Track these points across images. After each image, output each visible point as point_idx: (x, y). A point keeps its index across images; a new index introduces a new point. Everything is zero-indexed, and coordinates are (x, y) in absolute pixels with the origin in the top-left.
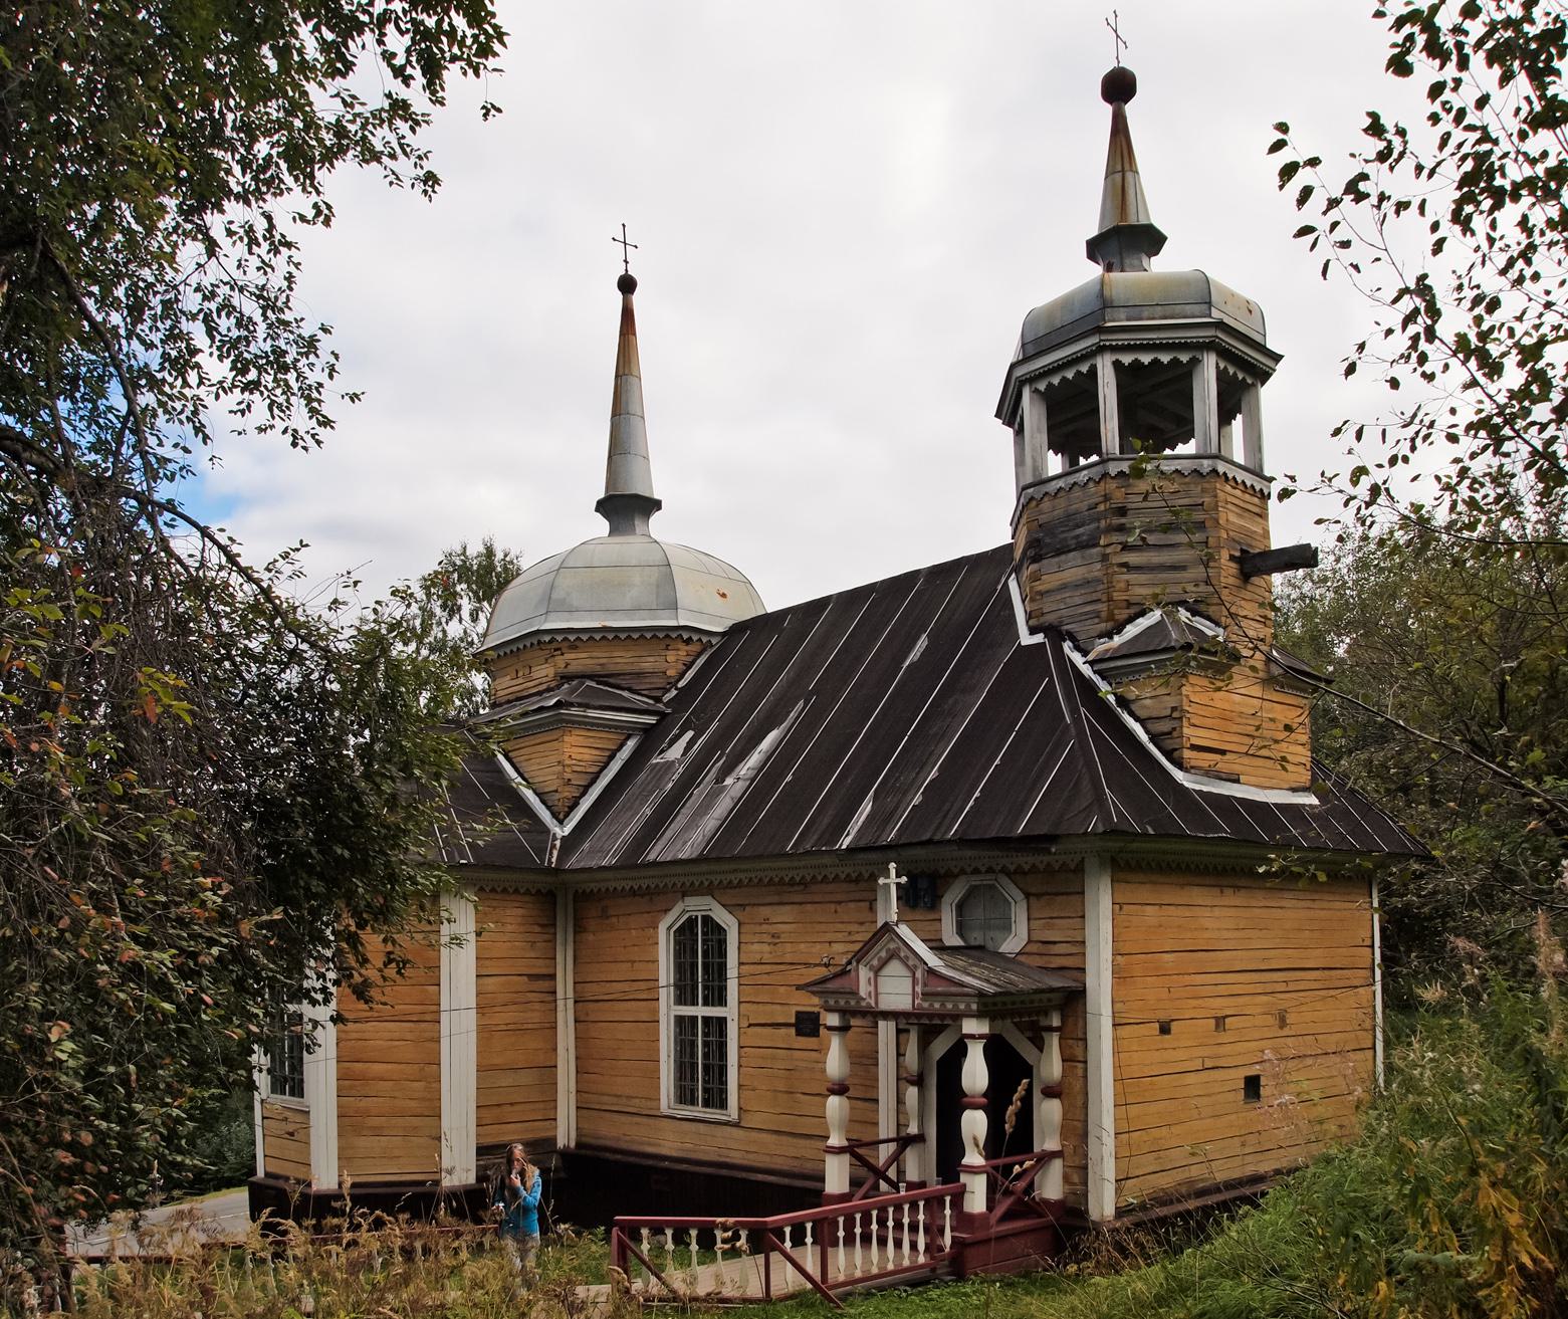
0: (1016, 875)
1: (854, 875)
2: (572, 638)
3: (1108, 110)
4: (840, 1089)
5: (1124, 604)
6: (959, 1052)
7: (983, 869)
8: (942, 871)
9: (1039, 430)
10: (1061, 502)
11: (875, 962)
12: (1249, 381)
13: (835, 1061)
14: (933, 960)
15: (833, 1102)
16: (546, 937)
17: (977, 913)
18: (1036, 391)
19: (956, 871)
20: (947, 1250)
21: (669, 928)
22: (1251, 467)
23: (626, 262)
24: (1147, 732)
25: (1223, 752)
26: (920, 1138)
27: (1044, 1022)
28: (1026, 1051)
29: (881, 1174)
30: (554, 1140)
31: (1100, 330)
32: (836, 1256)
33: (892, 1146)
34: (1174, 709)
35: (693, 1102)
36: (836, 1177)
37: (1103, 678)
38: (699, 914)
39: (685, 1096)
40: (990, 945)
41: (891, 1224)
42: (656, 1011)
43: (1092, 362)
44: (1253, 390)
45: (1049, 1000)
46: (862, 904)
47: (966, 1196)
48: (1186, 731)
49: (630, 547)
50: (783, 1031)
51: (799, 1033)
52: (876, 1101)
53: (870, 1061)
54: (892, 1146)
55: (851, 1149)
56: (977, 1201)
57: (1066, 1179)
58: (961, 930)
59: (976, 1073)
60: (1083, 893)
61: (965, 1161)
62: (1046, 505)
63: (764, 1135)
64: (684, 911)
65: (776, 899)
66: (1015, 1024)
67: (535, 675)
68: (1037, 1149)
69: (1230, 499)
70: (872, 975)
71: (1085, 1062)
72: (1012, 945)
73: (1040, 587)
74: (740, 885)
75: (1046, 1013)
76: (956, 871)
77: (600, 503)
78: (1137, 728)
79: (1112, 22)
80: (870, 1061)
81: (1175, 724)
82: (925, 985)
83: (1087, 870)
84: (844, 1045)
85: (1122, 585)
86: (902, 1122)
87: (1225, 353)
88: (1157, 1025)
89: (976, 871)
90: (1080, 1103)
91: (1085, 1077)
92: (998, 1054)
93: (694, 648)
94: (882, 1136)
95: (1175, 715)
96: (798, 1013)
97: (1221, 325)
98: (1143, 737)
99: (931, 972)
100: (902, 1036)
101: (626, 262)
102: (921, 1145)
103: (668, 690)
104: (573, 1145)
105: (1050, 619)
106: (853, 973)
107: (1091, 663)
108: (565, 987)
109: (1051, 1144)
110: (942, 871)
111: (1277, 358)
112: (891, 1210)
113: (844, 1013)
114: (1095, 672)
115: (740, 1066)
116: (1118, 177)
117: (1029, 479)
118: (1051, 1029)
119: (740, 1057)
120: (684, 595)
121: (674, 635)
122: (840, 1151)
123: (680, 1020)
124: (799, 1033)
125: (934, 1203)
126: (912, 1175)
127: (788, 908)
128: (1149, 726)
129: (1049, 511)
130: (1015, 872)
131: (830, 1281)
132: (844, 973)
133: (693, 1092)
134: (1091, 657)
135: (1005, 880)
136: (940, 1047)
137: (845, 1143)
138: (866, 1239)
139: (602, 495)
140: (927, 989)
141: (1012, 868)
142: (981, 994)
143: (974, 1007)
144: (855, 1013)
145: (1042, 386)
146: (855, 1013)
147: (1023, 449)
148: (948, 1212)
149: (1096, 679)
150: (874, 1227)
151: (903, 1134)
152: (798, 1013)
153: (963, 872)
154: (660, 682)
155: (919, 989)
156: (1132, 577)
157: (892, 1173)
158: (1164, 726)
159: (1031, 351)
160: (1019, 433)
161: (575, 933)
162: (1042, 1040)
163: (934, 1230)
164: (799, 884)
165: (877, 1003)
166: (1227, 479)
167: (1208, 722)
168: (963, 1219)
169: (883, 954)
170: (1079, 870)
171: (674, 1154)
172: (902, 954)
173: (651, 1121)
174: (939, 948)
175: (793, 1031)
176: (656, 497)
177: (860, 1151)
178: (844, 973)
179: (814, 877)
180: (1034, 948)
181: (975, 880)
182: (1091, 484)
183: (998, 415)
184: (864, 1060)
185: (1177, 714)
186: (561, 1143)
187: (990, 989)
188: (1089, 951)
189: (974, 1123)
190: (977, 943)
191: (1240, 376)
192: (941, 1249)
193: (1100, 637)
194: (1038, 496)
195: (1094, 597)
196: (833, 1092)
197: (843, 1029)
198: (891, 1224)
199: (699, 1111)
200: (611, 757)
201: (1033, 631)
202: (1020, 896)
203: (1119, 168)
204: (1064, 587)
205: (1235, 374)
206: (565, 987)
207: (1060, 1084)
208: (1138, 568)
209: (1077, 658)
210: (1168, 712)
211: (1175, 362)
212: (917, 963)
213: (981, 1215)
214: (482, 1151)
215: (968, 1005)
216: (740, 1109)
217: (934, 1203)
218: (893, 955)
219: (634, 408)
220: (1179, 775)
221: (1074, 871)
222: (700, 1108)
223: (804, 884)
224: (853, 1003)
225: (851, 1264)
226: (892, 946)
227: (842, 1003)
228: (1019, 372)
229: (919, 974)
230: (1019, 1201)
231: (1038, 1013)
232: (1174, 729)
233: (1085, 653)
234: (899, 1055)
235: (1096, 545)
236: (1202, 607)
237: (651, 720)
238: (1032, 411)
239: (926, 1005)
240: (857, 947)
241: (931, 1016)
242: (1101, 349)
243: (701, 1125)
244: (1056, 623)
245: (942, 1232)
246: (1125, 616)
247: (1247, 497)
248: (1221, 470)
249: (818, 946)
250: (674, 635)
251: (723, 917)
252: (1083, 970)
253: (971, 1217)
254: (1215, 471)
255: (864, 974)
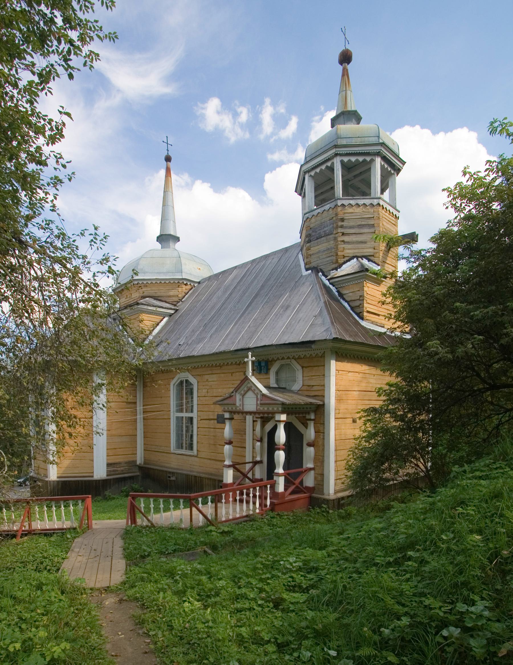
0: (298, 359)
1: (238, 362)
2: (145, 282)
3: (340, 68)
4: (230, 443)
5: (342, 257)
6: (275, 429)
7: (286, 358)
8: (270, 359)
9: (311, 192)
10: (319, 218)
11: (242, 392)
12: (392, 172)
13: (227, 430)
14: (265, 391)
15: (227, 447)
16: (133, 389)
17: (283, 375)
18: (311, 176)
19: (275, 359)
20: (268, 507)
21: (174, 385)
22: (391, 204)
23: (168, 150)
24: (350, 306)
25: (379, 315)
26: (261, 462)
27: (308, 417)
28: (300, 427)
29: (245, 476)
30: (136, 461)
31: (336, 146)
32: (222, 508)
33: (251, 465)
34: (360, 296)
35: (182, 448)
36: (229, 476)
37: (334, 286)
38: (184, 379)
39: (180, 446)
40: (288, 388)
41: (251, 495)
42: (169, 415)
43: (332, 161)
44: (393, 176)
45: (310, 408)
46: (241, 373)
47: (276, 485)
48: (365, 305)
49: (167, 252)
50: (212, 421)
51: (218, 422)
52: (245, 448)
53: (243, 433)
54: (251, 465)
55: (233, 466)
56: (281, 488)
57: (315, 478)
58: (277, 381)
59: (281, 436)
60: (324, 366)
61: (276, 471)
62: (313, 220)
63: (206, 460)
64: (179, 378)
65: (210, 372)
66: (296, 417)
67: (133, 296)
68: (304, 467)
69: (384, 216)
70: (241, 397)
71: (324, 433)
72: (296, 387)
73: (310, 252)
74: (198, 367)
75: (309, 413)
76: (275, 359)
77: (158, 238)
78: (346, 305)
79: (343, 30)
80: (243, 433)
81: (361, 302)
82: (261, 400)
83: (326, 355)
84: (231, 425)
85: (342, 249)
86: (255, 455)
87: (384, 159)
88: (352, 419)
89: (283, 359)
90: (321, 449)
91: (324, 439)
92: (289, 427)
93: (189, 287)
94: (247, 461)
95: (361, 298)
96: (218, 415)
97: (383, 144)
98: (348, 308)
99: (263, 395)
100: (255, 423)
101: (168, 150)
102: (261, 465)
103: (179, 302)
104: (142, 463)
105: (313, 265)
106: (234, 397)
107: (329, 280)
108: (140, 408)
109: (311, 465)
110: (270, 359)
111: (404, 163)
112: (251, 490)
113: (231, 412)
114: (330, 284)
115: (198, 435)
116: (344, 93)
117: (307, 211)
118: (310, 420)
119: (197, 431)
120: (185, 268)
121: (181, 282)
122: (229, 466)
123: (177, 418)
124: (218, 422)
125: (263, 488)
126: (258, 476)
127: (215, 375)
128: (351, 303)
129: (314, 223)
130: (298, 358)
131: (219, 520)
132: (231, 396)
133: (182, 444)
134: (329, 277)
135: (294, 361)
136: (269, 427)
137: (231, 463)
138: (241, 501)
139: (158, 234)
140: (262, 402)
141: (297, 357)
142: (283, 404)
143: (280, 409)
144: (234, 413)
145: (312, 173)
146: (234, 413)
147: (305, 204)
148: (269, 492)
149: (331, 286)
150: (245, 496)
151: (254, 460)
152: (218, 415)
153: (278, 359)
154: (176, 299)
155: (259, 402)
156: (346, 246)
157: (250, 475)
158: (357, 303)
159: (308, 159)
160: (304, 197)
161: (144, 387)
162: (307, 424)
163: (263, 498)
164: (219, 366)
165: (243, 408)
166: (383, 208)
167: (373, 303)
168: (275, 495)
169: (246, 389)
170: (323, 356)
171: (175, 467)
172: (253, 388)
173: (168, 455)
174: (267, 387)
175: (216, 421)
176: (178, 236)
177: (237, 466)
178: (231, 396)
179: (224, 363)
180: (305, 388)
181: (283, 362)
182: (331, 210)
183: (296, 191)
184: (240, 432)
185: (361, 298)
186: (138, 463)
187: (287, 402)
188: (326, 389)
189: (281, 456)
190: (283, 386)
191: (389, 169)
192: (266, 506)
193: (333, 270)
194: (310, 217)
195: (331, 254)
196: (227, 444)
197: (231, 419)
198: (251, 495)
199: (183, 451)
200: (158, 324)
201: (307, 270)
202: (299, 368)
203: (345, 89)
204: (319, 252)
205: (387, 168)
206: (140, 408)
207: (314, 442)
208: (348, 243)
209: (323, 278)
210: (358, 298)
211: (364, 161)
212: (259, 392)
213: (282, 493)
214: (109, 465)
215: (278, 409)
216: (198, 450)
217: (263, 488)
218: (249, 389)
219: (170, 203)
220: (363, 323)
221: (321, 357)
222: (184, 450)
223: (220, 366)
224: (234, 408)
225: (227, 513)
226: (249, 385)
227: (230, 408)
228: (305, 168)
229: (259, 397)
230: (297, 487)
231: (306, 413)
232: (360, 304)
233: (326, 276)
234: (254, 430)
235: (331, 234)
236: (372, 258)
237: (172, 312)
238: (309, 186)
239: (261, 409)
240: (236, 386)
241: (263, 413)
242: (336, 155)
243: (185, 457)
244: (316, 266)
245: (266, 498)
246: (343, 261)
247: (390, 217)
248: (381, 204)
249: (225, 389)
250: (181, 282)
251: (193, 380)
252: (324, 396)
253: (278, 494)
254: (379, 204)
255: (238, 397)
